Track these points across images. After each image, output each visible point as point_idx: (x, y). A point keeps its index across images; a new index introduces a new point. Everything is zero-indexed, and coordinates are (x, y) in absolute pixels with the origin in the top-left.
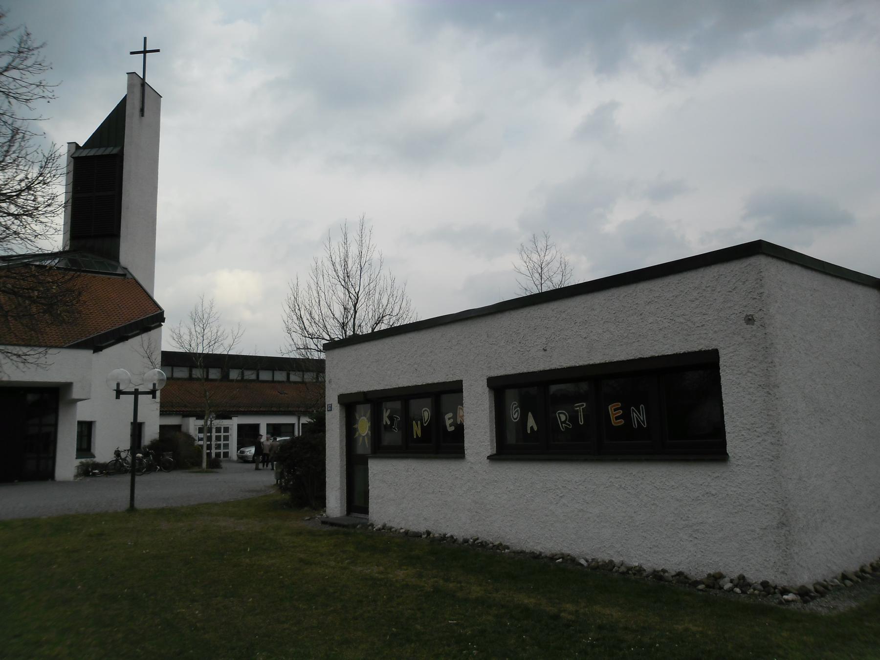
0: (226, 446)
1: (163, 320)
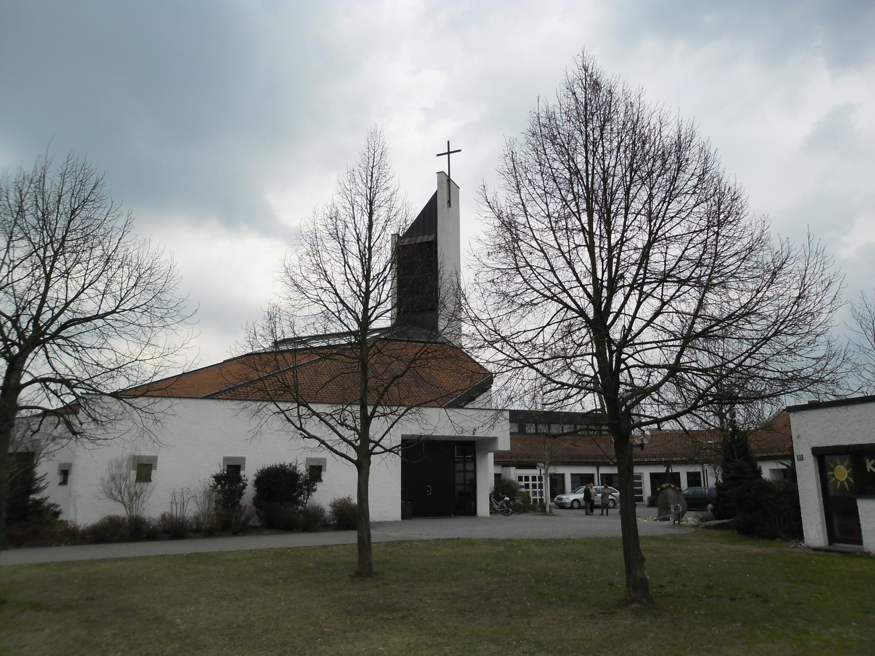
0: (541, 493)
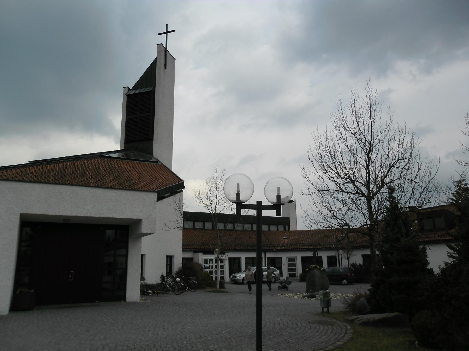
0: (222, 272)
1: (184, 187)
